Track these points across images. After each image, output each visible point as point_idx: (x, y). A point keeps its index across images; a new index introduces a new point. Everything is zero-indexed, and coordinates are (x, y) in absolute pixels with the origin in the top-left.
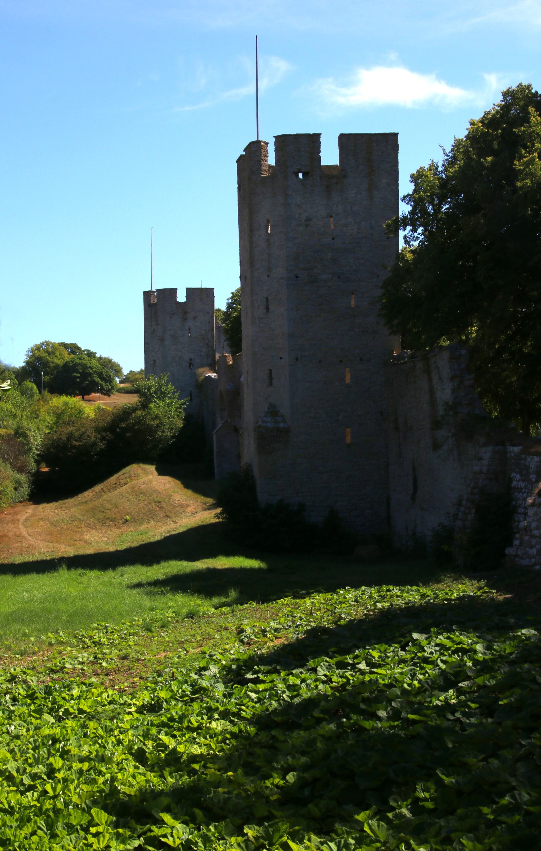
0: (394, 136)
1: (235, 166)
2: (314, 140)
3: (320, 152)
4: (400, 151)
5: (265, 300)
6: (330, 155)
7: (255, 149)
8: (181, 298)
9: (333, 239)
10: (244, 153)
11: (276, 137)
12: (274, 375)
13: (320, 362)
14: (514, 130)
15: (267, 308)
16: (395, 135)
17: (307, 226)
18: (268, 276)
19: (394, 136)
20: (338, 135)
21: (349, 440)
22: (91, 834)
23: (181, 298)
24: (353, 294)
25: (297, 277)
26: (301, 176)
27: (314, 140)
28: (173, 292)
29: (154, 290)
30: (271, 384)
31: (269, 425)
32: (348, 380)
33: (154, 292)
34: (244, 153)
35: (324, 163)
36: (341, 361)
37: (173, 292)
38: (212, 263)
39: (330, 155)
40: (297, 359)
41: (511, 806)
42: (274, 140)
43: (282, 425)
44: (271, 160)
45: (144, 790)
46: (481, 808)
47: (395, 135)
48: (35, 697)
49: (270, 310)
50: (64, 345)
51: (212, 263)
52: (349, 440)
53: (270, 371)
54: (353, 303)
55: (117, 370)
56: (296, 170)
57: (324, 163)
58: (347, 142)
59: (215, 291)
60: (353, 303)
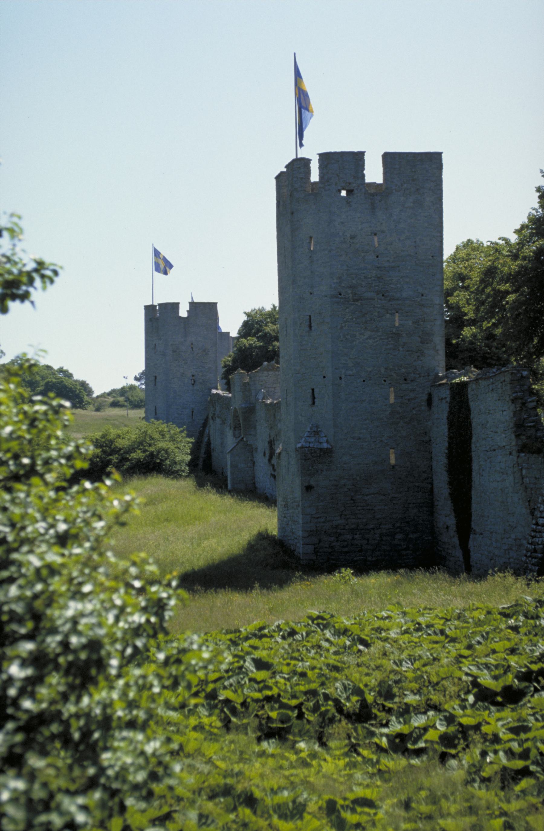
0: (438, 155)
1: (274, 181)
2: (357, 158)
3: (364, 169)
4: (444, 171)
5: (308, 317)
6: (374, 173)
7: (299, 166)
8: (183, 312)
9: (377, 257)
10: (285, 170)
11: (321, 155)
12: (316, 395)
13: (364, 381)
15: (310, 326)
16: (439, 154)
19: (438, 155)
20: (382, 153)
21: (393, 461)
22: (284, 788)
23: (183, 312)
26: (344, 193)
27: (357, 158)
28: (175, 306)
29: (155, 304)
33: (156, 306)
34: (285, 170)
35: (368, 180)
37: (175, 306)
38: (241, 280)
39: (374, 173)
42: (318, 157)
43: (325, 446)
44: (315, 177)
45: (249, 794)
47: (439, 154)
49: (313, 328)
51: (241, 280)
52: (393, 461)
55: (90, 392)
56: (340, 188)
57: (368, 180)
58: (390, 160)
59: (218, 305)
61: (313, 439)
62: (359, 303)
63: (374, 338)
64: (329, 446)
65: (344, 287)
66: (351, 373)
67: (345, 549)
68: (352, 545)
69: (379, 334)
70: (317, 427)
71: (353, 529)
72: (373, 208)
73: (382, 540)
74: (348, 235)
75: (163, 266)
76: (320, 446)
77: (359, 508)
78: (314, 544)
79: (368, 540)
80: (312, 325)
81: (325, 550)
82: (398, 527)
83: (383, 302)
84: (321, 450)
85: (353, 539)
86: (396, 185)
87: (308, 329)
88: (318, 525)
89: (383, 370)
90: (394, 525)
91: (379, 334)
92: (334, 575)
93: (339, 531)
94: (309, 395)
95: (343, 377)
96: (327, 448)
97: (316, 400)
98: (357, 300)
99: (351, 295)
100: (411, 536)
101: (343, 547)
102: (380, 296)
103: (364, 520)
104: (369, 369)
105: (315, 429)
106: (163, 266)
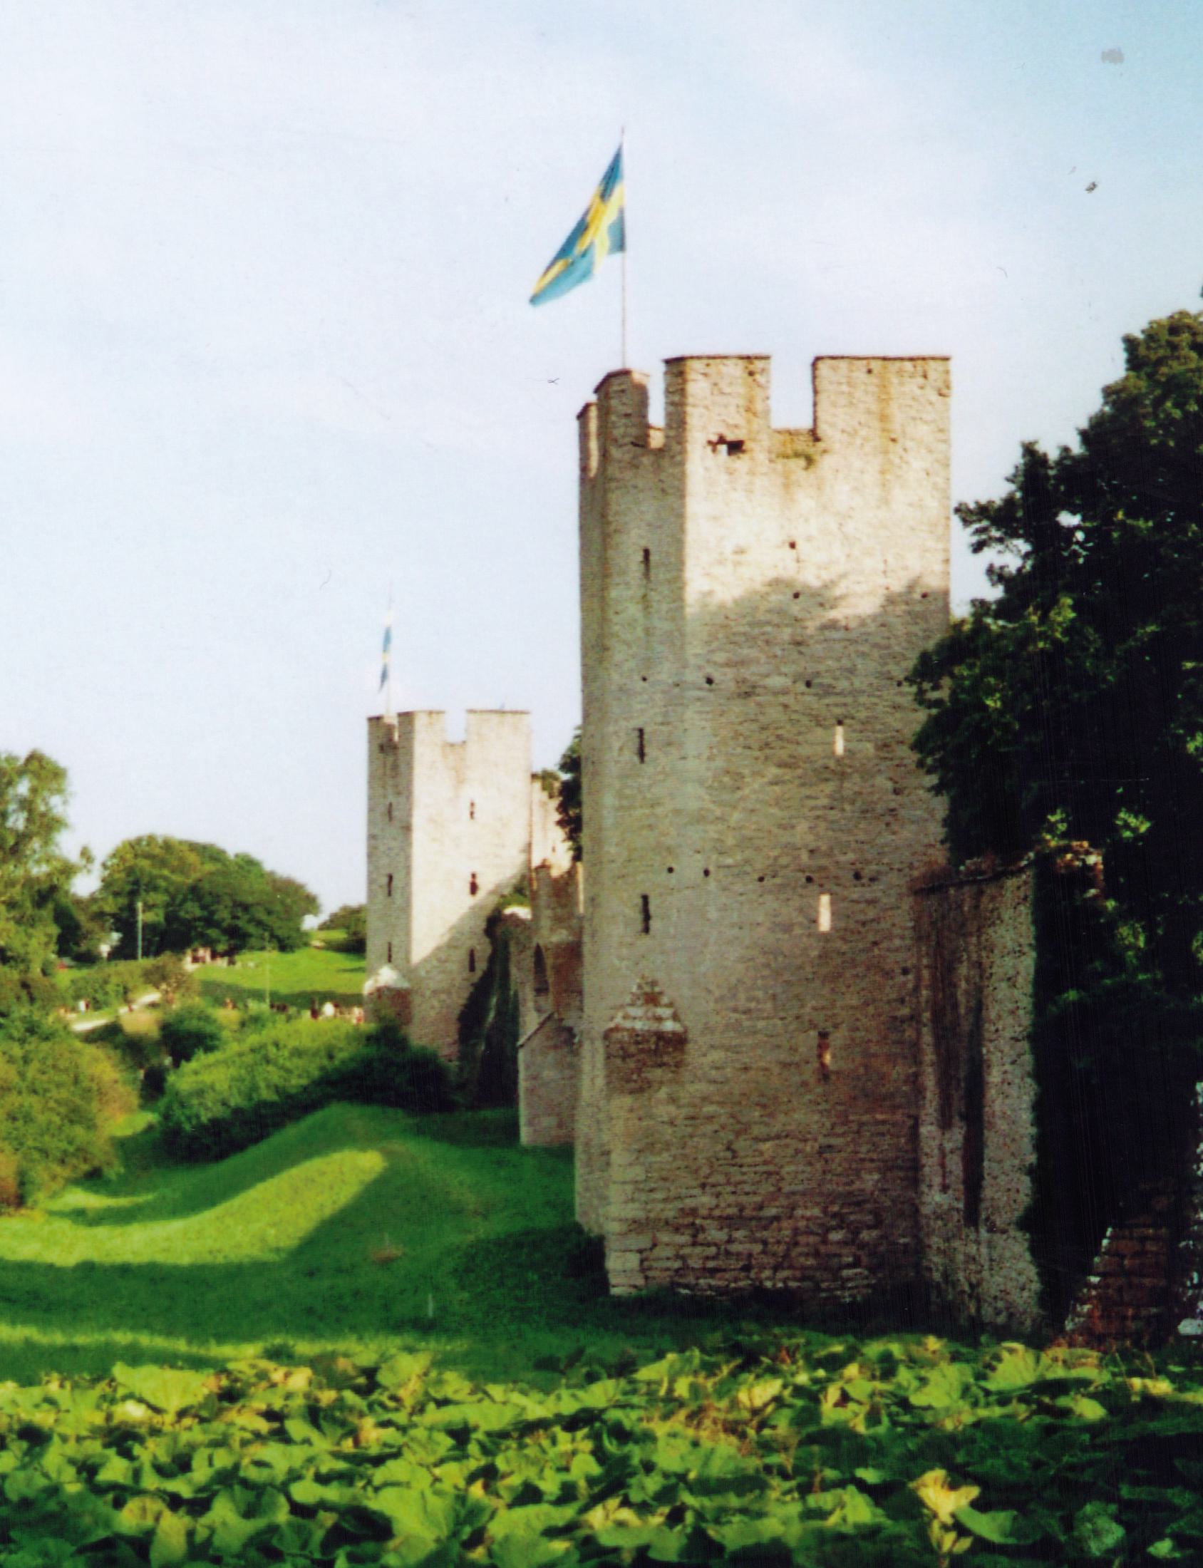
5: (637, 733)
13: (761, 879)
14: (1151, 1550)
15: (642, 754)
17: (737, 564)
24: (840, 723)
25: (710, 681)
30: (646, 930)
31: (639, 1025)
32: (825, 922)
36: (809, 880)
40: (707, 873)
41: (1141, 1472)
43: (669, 1026)
46: (1151, 1550)
48: (1189, 1552)
49: (646, 759)
50: (194, 847)
53: (645, 899)
54: (840, 748)
55: (310, 903)
60: (840, 748)
63: (784, 782)
66: (730, 861)
82: (834, 1215)
84: (660, 1036)
87: (636, 759)
96: (674, 1033)
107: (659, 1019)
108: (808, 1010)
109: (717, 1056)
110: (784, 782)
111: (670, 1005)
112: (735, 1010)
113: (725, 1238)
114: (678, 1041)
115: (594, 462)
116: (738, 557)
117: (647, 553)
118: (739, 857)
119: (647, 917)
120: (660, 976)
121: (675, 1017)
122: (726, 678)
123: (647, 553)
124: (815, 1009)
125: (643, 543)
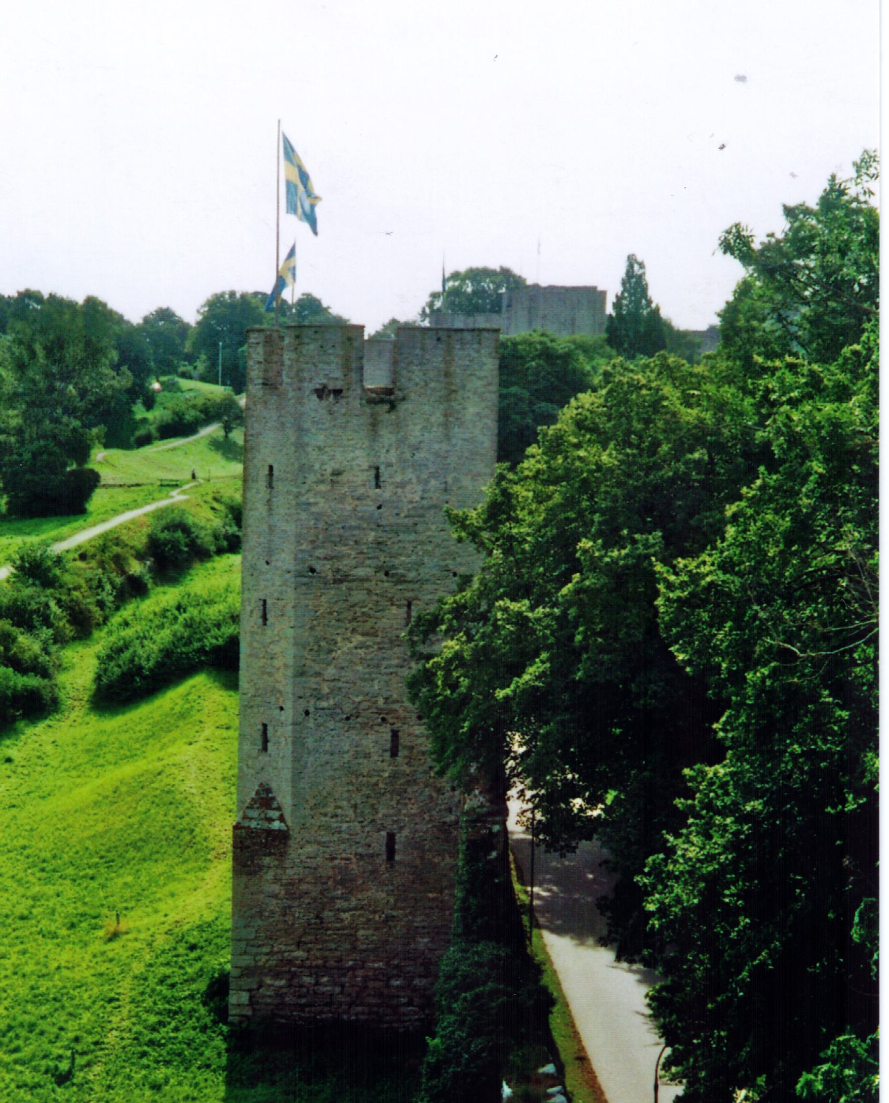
13: (348, 719)
15: (265, 618)
18: (267, 563)
30: (265, 749)
31: (253, 824)
40: (307, 713)
43: (276, 825)
61: (254, 814)
62: (344, 586)
63: (368, 647)
64: (283, 827)
65: (319, 558)
66: (324, 704)
67: (303, 1001)
68: (315, 993)
69: (378, 640)
70: (269, 791)
71: (317, 966)
72: (374, 425)
73: (366, 987)
74: (329, 471)
75: (301, 196)
76: (266, 825)
77: (329, 932)
78: (250, 990)
79: (343, 986)
80: (268, 616)
81: (269, 1000)
82: (397, 966)
83: (386, 584)
84: (269, 832)
85: (317, 983)
86: (417, 384)
87: (260, 621)
88: (258, 958)
89: (381, 702)
90: (388, 964)
91: (378, 640)
92: (761, 243)
93: (293, 969)
94: (258, 736)
95: (311, 710)
96: (279, 831)
97: (269, 745)
98: (341, 581)
99: (330, 574)
100: (416, 982)
101: (300, 997)
102: (381, 575)
103: (337, 954)
104: (358, 700)
105: (263, 795)
106: (301, 196)
107: (270, 820)
108: (380, 815)
109: (310, 849)
110: (368, 647)
111: (279, 809)
112: (325, 815)
113: (313, 981)
114: (283, 837)
115: (299, 204)
116: (334, 478)
117: (271, 468)
118: (332, 702)
119: (265, 741)
120: (274, 785)
121: (282, 819)
122: (325, 568)
123: (271, 468)
124: (386, 816)
125: (270, 461)
